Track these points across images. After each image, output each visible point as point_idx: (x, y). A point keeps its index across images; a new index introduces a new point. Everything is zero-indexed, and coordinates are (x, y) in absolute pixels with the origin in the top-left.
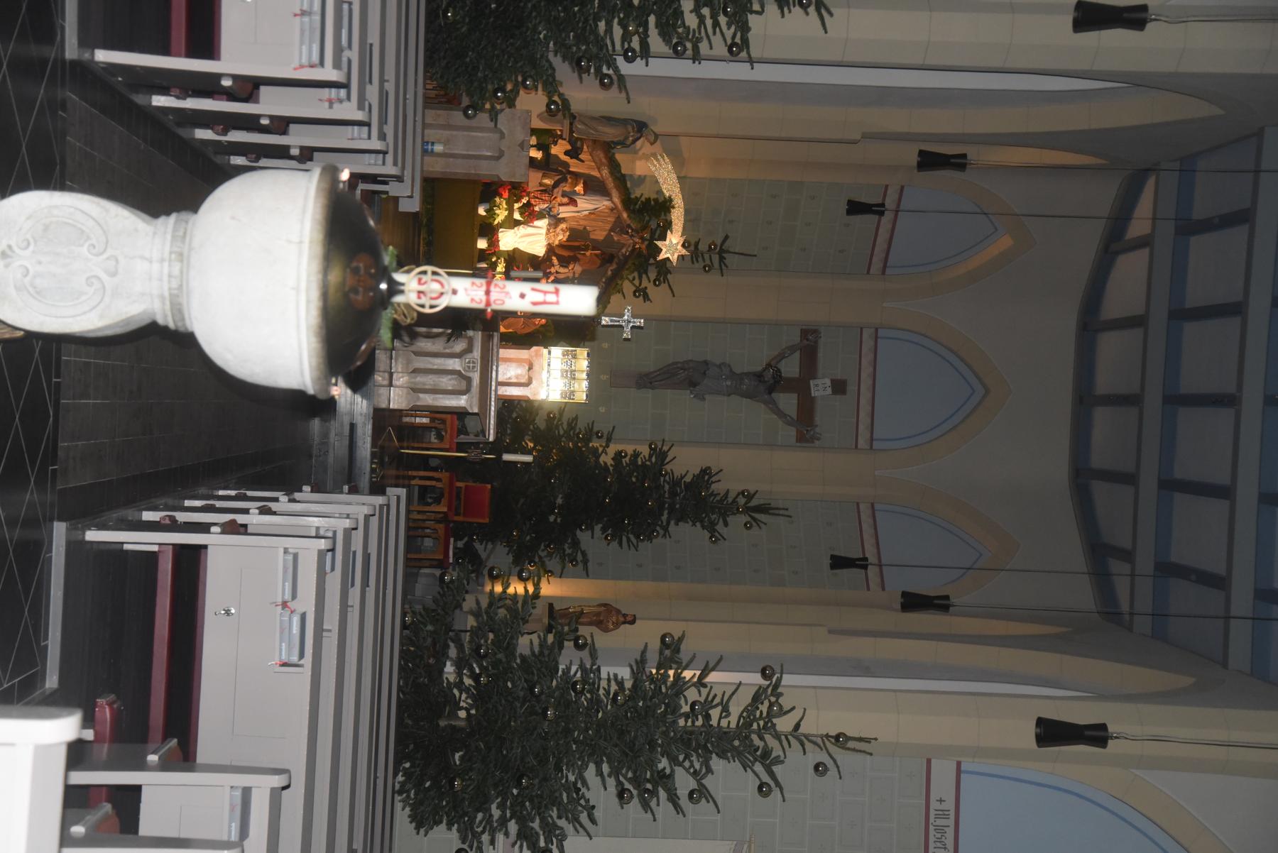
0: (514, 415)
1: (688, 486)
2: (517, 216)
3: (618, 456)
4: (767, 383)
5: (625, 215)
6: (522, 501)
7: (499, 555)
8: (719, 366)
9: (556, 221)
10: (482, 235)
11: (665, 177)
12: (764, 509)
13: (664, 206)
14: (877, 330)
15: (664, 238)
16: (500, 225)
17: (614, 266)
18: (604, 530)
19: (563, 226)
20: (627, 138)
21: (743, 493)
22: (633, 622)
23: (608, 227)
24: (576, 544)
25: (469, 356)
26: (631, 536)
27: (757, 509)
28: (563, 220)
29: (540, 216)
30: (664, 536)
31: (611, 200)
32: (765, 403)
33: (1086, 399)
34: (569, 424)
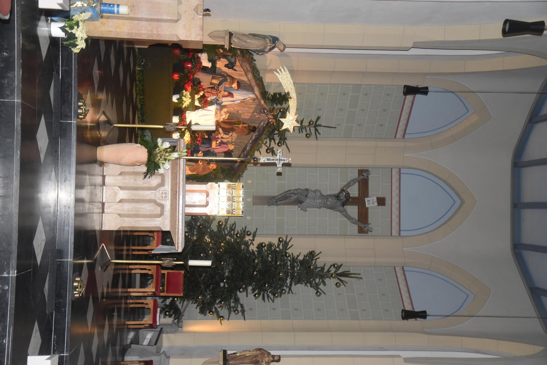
0: (198, 224)
1: (302, 262)
2: (197, 103)
3: (260, 246)
4: (342, 200)
5: (262, 102)
6: (204, 275)
7: (192, 308)
8: (315, 191)
9: (222, 107)
10: (175, 114)
11: (285, 81)
12: (346, 274)
13: (283, 98)
14: (400, 169)
15: (284, 117)
16: (187, 109)
17: (256, 133)
18: (253, 290)
19: (225, 110)
20: (265, 48)
21: (334, 265)
22: (278, 361)
23: (252, 111)
24: (237, 300)
25: (162, 189)
26: (270, 294)
27: (341, 274)
28: (225, 106)
29: (211, 103)
30: (289, 293)
31: (254, 94)
32: (341, 212)
33: (518, 205)
34: (231, 228)
